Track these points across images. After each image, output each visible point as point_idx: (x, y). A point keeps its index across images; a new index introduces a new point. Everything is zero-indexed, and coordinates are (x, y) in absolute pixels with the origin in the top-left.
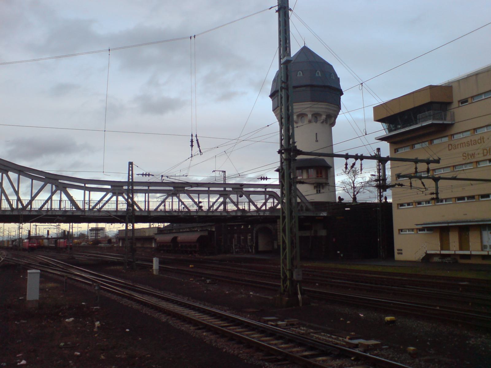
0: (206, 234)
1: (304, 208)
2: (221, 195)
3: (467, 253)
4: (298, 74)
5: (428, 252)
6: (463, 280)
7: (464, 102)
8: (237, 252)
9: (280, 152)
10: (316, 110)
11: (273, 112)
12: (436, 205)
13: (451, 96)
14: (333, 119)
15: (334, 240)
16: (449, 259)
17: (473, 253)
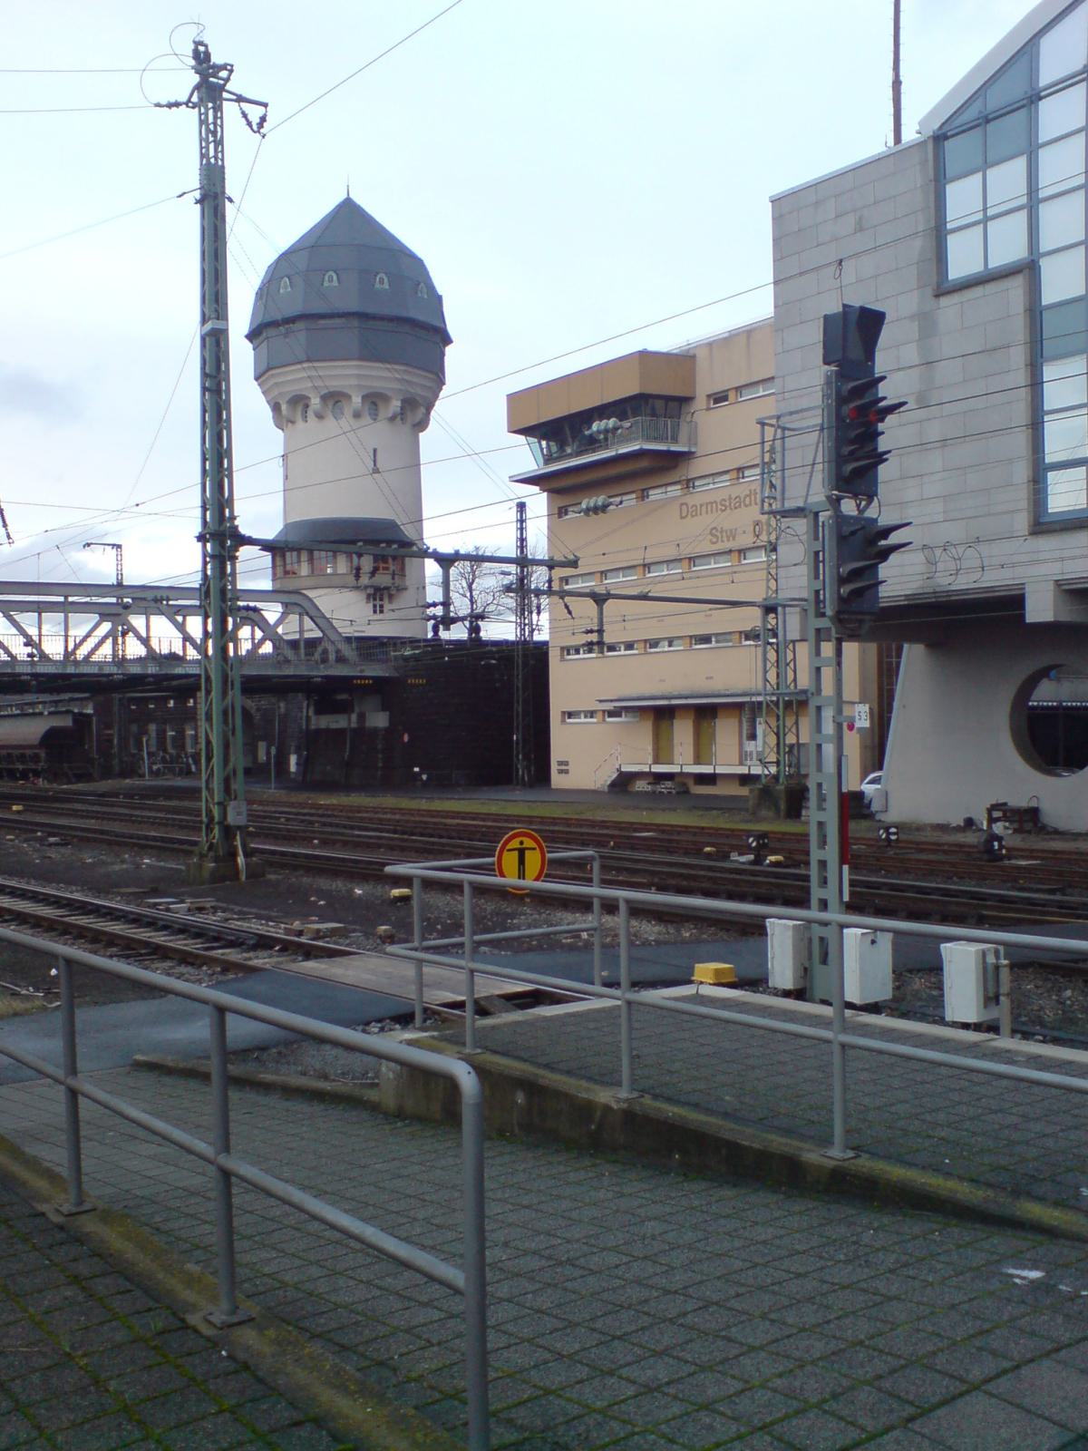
0: (67, 722)
1: (332, 657)
2: (104, 617)
3: (707, 769)
4: (326, 278)
5: (625, 769)
6: (646, 827)
7: (720, 398)
8: (157, 774)
9: (201, 538)
10: (378, 385)
11: (256, 383)
12: (646, 653)
13: (691, 379)
14: (423, 410)
15: (406, 738)
16: (669, 784)
17: (719, 770)
